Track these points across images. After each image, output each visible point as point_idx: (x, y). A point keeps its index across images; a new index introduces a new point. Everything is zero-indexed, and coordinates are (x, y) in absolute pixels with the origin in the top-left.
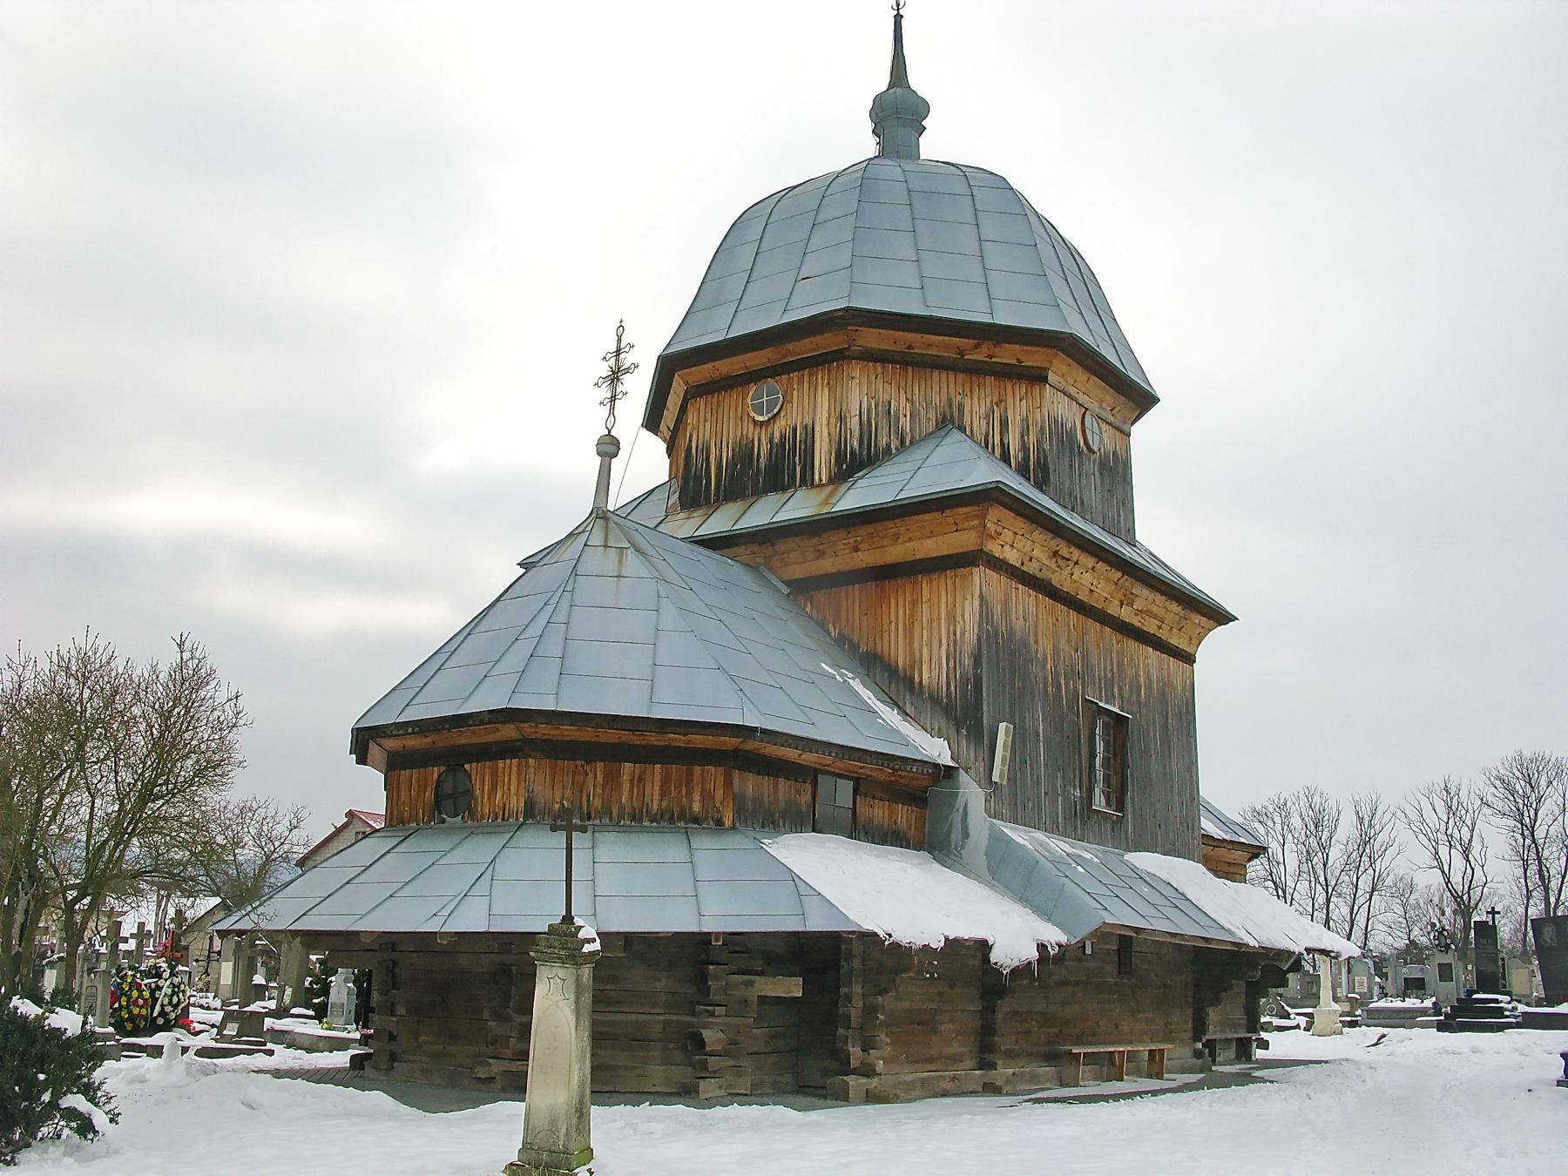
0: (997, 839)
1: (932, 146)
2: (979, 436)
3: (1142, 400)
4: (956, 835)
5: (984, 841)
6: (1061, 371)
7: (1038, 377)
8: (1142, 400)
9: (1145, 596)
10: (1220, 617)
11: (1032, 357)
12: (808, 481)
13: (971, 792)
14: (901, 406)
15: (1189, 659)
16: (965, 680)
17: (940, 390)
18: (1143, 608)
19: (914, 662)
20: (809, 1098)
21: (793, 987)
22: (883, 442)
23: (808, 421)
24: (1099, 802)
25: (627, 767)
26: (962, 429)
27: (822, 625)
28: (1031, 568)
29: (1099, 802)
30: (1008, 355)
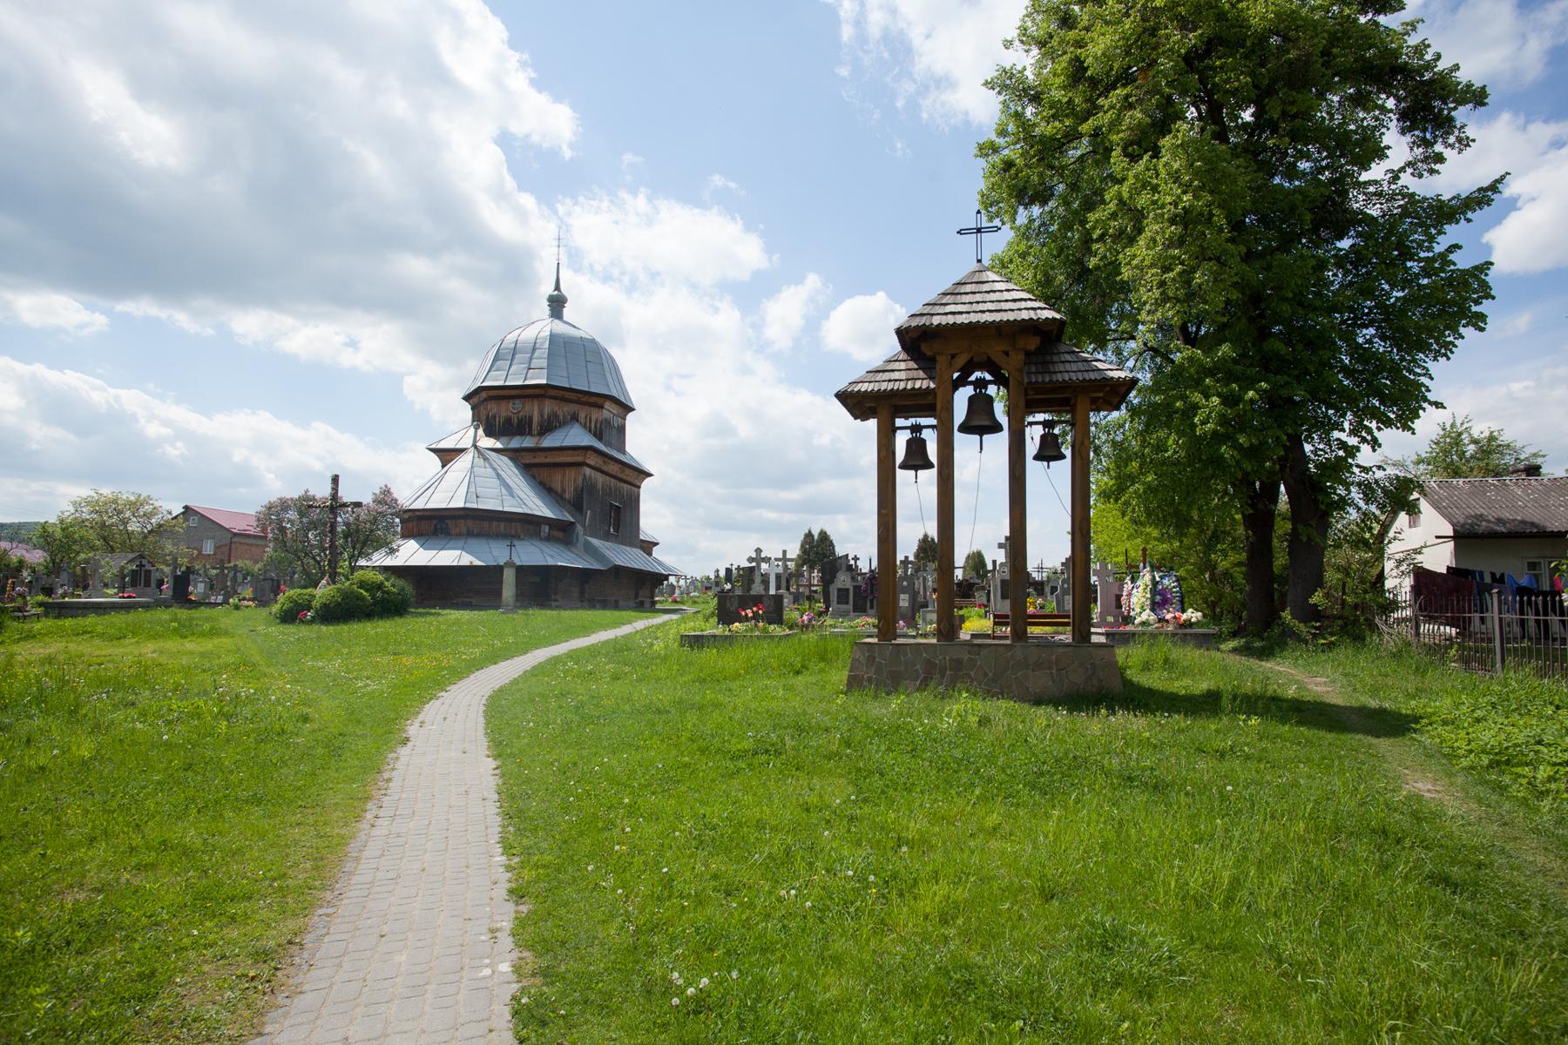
0: (586, 541)
3: (628, 409)
6: (608, 405)
7: (601, 407)
9: (628, 471)
11: (599, 401)
13: (579, 528)
15: (639, 487)
17: (572, 408)
18: (628, 473)
20: (476, 612)
21: (538, 579)
24: (612, 530)
25: (495, 523)
26: (577, 421)
27: (534, 477)
29: (612, 530)
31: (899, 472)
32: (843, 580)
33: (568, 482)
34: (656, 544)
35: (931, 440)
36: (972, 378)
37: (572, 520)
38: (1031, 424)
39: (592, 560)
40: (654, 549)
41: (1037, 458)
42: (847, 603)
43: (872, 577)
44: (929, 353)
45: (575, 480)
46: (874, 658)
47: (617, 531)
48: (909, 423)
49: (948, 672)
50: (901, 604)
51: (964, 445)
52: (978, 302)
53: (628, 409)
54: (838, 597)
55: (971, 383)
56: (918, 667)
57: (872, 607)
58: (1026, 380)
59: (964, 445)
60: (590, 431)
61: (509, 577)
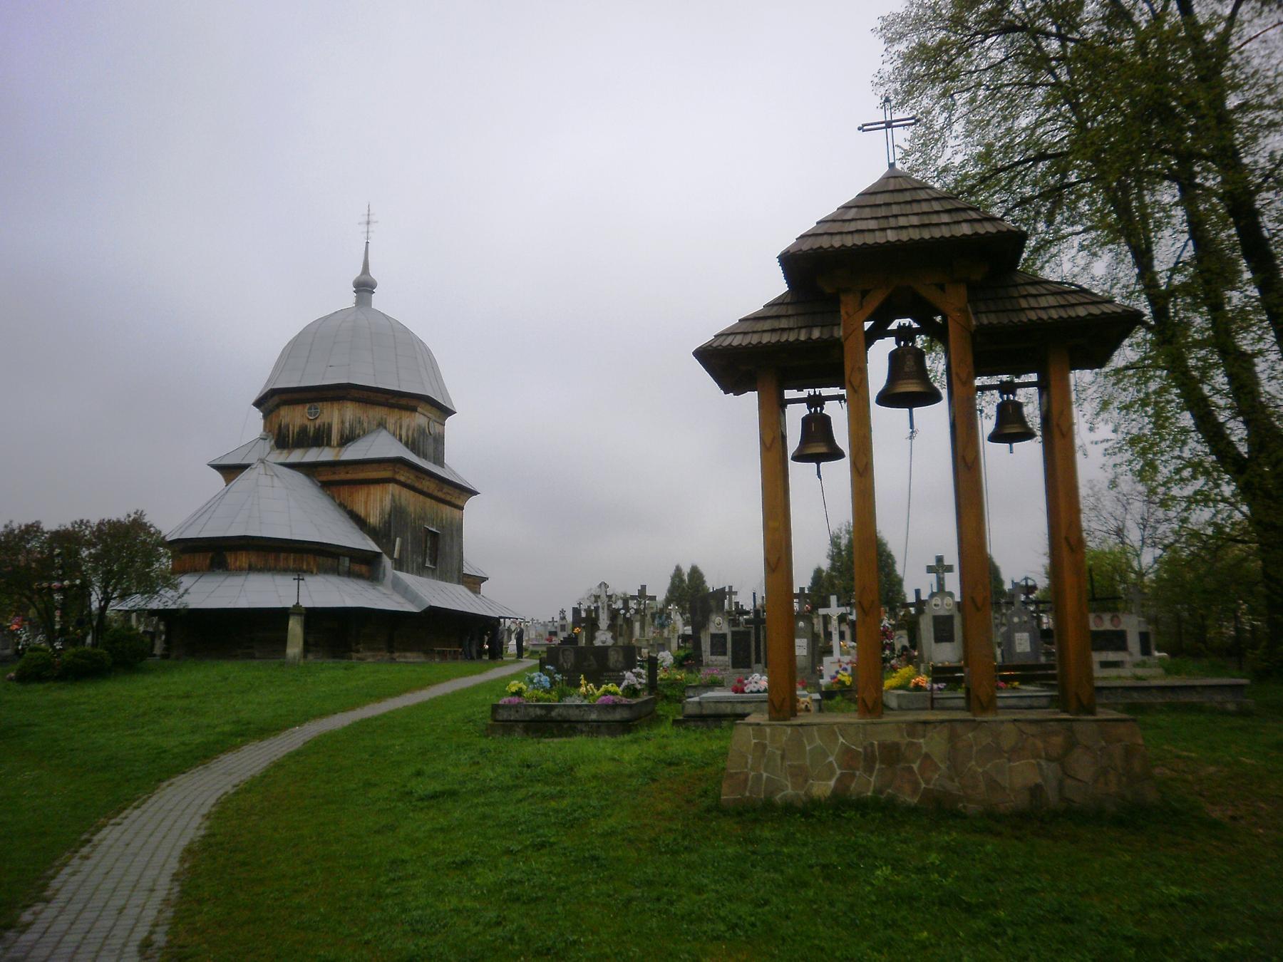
1: (379, 301)
2: (392, 430)
3: (446, 412)
4: (381, 576)
5: (391, 577)
7: (414, 410)
8: (448, 412)
10: (474, 493)
12: (329, 444)
13: (387, 562)
14: (364, 418)
15: (462, 508)
16: (385, 522)
17: (377, 413)
19: (368, 515)
22: (357, 432)
23: (330, 420)
26: (385, 428)
27: (333, 498)
28: (409, 482)
30: (403, 402)
31: (791, 464)
32: (718, 624)
33: (376, 502)
34: (484, 579)
35: (837, 413)
36: (894, 326)
37: (378, 550)
38: (983, 388)
39: (402, 600)
40: (300, 604)
41: (995, 438)
42: (724, 654)
43: (758, 618)
44: (828, 290)
45: (381, 501)
46: (764, 746)
47: (435, 564)
48: (805, 393)
49: (877, 766)
50: (798, 652)
51: (887, 421)
52: (896, 216)
53: (446, 412)
54: (713, 645)
55: (891, 333)
56: (831, 759)
57: (758, 661)
58: (974, 323)
59: (887, 421)
60: (400, 440)
61: (295, 627)
